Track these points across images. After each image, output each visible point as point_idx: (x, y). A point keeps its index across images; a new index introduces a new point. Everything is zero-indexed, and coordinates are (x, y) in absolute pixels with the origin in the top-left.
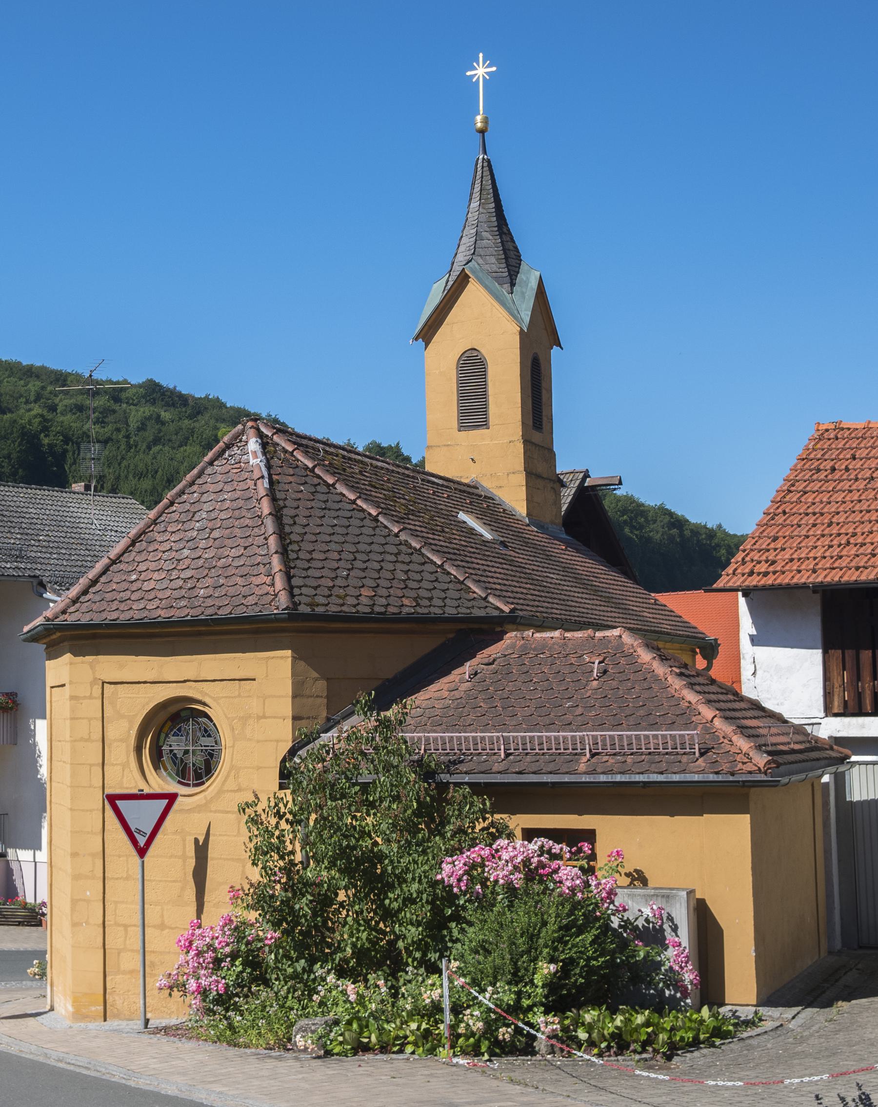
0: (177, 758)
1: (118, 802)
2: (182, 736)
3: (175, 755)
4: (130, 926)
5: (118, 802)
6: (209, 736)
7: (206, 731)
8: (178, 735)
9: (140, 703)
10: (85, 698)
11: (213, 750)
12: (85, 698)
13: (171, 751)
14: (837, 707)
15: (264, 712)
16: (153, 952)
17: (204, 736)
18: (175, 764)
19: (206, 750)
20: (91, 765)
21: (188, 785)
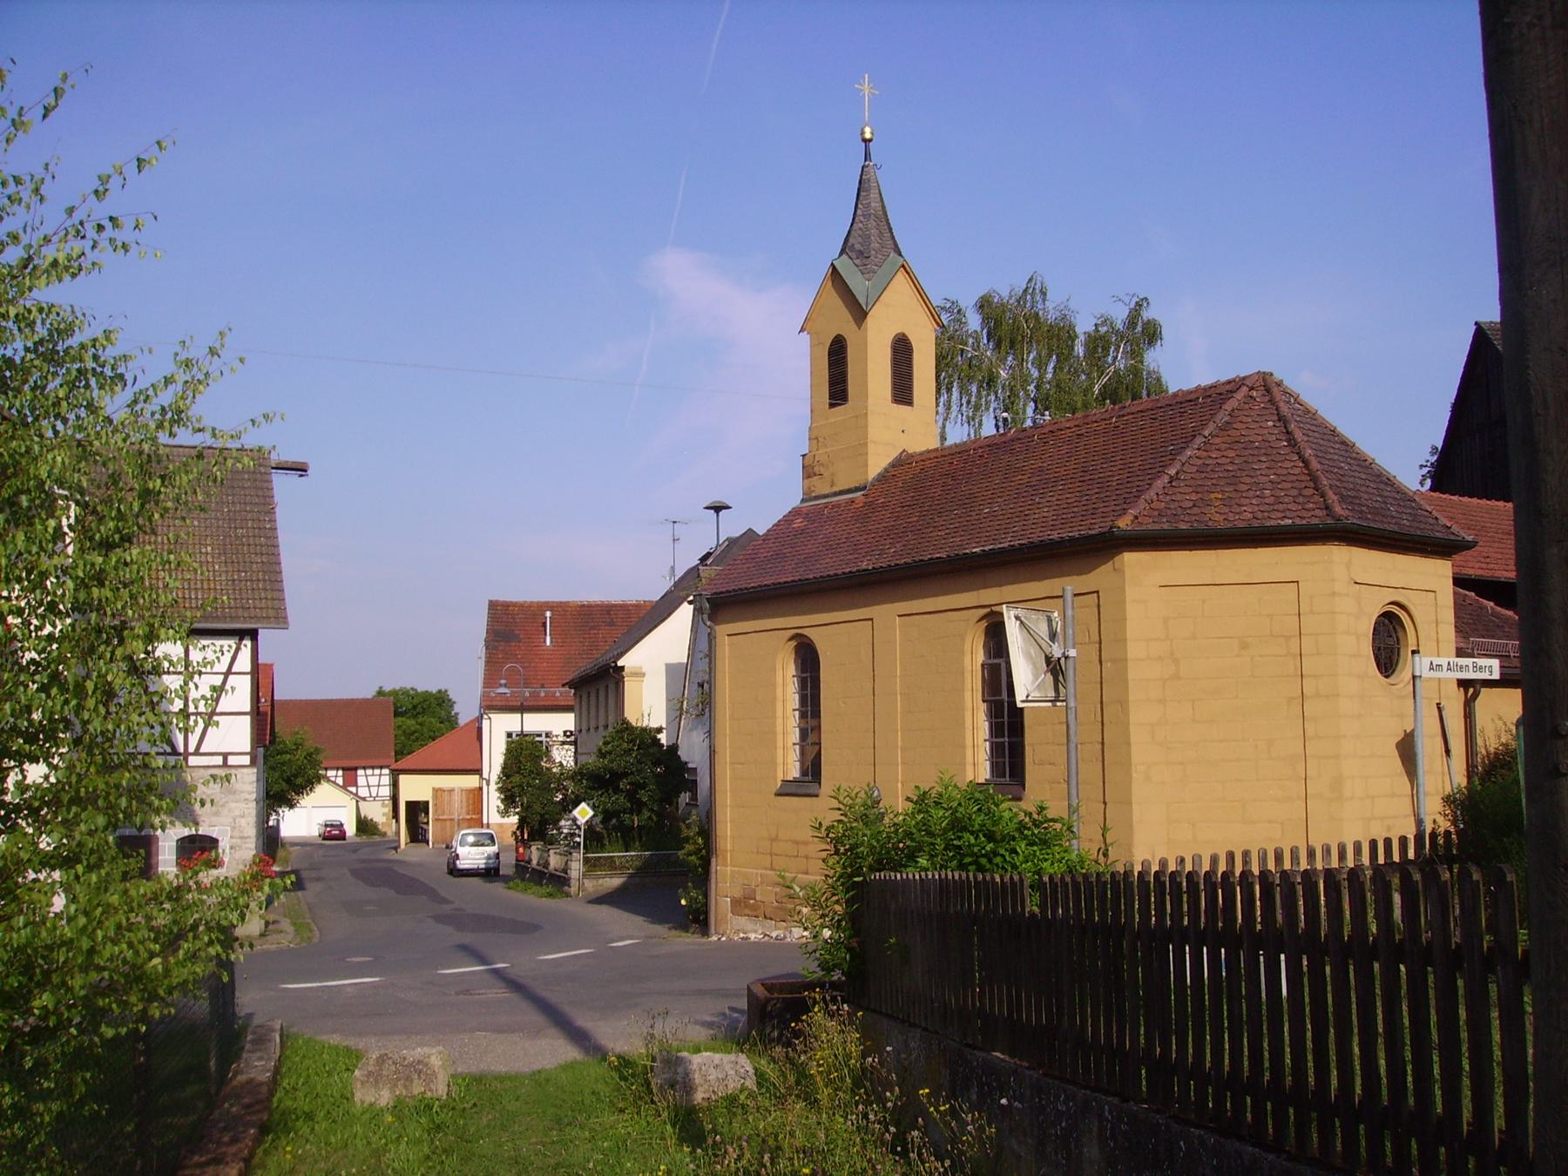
4: (710, 734)
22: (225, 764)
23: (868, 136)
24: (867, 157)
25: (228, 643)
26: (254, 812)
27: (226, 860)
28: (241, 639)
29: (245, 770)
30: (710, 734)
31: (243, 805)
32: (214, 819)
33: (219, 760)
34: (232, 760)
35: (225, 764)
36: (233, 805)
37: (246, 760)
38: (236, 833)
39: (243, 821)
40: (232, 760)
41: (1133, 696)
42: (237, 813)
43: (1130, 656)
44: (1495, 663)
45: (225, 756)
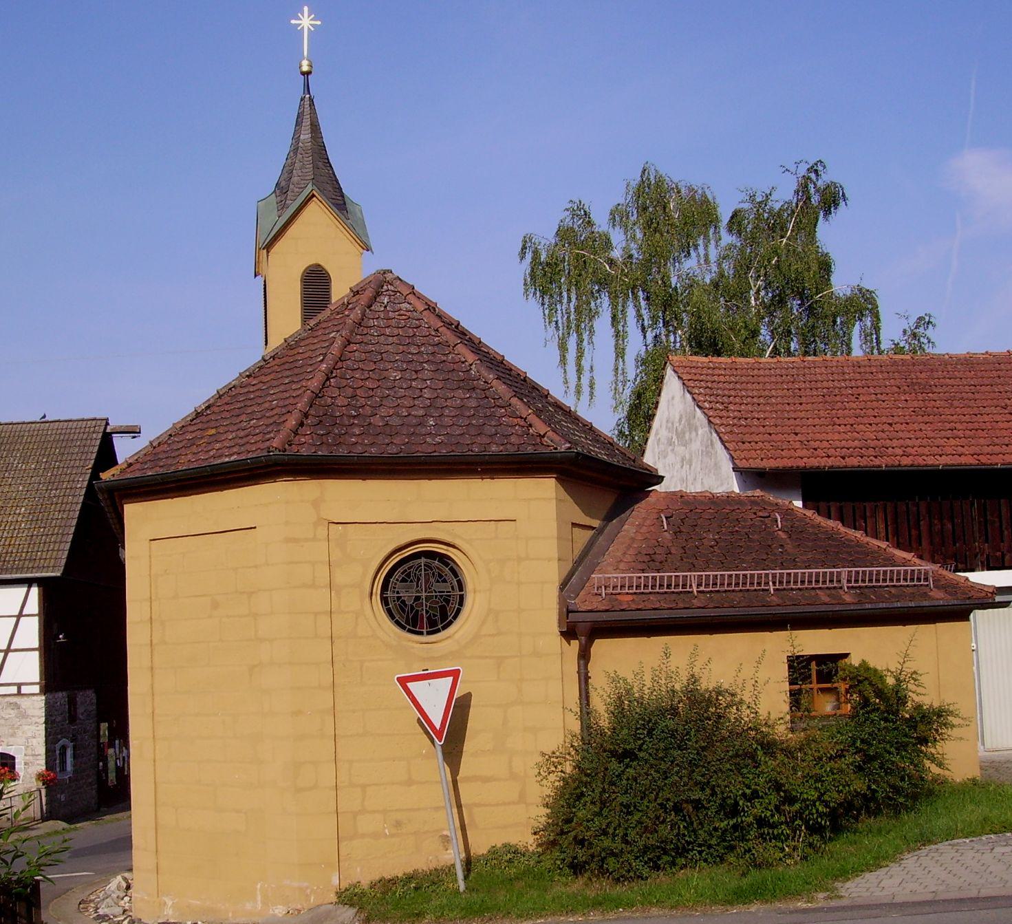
0: (406, 605)
1: (410, 685)
2: (411, 581)
3: (403, 602)
4: (369, 785)
5: (410, 685)
6: (445, 581)
7: (440, 576)
8: (407, 581)
9: (372, 552)
10: (306, 540)
11: (450, 596)
12: (306, 540)
13: (399, 598)
14: (982, 764)
15: (584, 656)
16: (344, 812)
17: (438, 582)
18: (404, 611)
19: (441, 596)
20: (316, 614)
21: (421, 633)
22: (19, 693)
23: (305, 68)
24: (307, 88)
25: (21, 591)
26: (43, 733)
27: (21, 774)
28: (30, 587)
29: (35, 698)
30: (369, 785)
31: (33, 728)
32: (11, 740)
33: (14, 690)
34: (24, 690)
35: (19, 693)
36: (26, 728)
37: (36, 689)
38: (29, 752)
39: (34, 741)
40: (24, 690)
41: (44, 757)
42: (30, 734)
43: (556, 541)
44: (102, 724)
45: (19, 686)
